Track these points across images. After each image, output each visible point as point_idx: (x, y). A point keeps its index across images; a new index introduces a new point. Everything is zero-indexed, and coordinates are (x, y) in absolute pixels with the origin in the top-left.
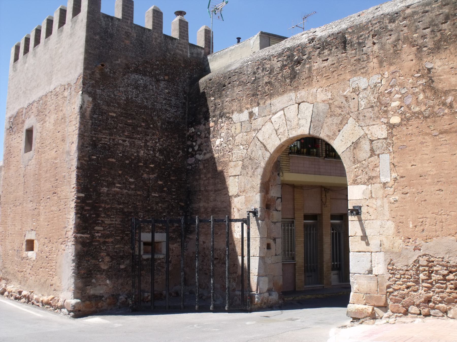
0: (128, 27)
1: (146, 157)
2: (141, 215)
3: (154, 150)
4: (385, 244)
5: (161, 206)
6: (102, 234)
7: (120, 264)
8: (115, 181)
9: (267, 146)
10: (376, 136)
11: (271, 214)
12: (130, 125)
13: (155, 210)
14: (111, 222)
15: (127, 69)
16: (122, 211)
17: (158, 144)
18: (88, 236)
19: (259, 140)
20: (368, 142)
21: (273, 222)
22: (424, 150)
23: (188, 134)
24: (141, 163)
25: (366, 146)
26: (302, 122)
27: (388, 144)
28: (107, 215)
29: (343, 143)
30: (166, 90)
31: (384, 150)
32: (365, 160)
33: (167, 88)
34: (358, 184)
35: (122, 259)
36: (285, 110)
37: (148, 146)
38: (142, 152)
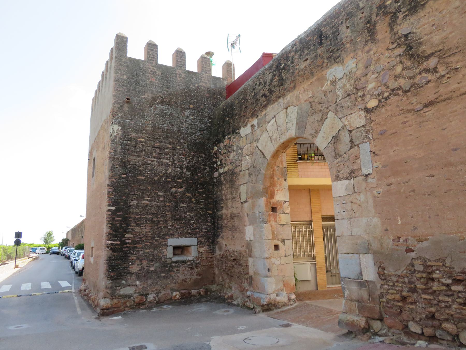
0: (153, 66)
1: (174, 173)
2: (169, 223)
3: (181, 167)
4: (373, 245)
5: (189, 215)
6: (132, 240)
7: (149, 267)
8: (144, 195)
9: (264, 153)
10: (355, 126)
12: (157, 148)
13: (183, 219)
15: (153, 101)
16: (151, 220)
17: (185, 163)
18: (118, 243)
20: (347, 134)
21: (280, 225)
23: (213, 152)
25: (345, 137)
26: (290, 125)
27: (367, 132)
29: (325, 139)
31: (364, 139)
32: (345, 153)
33: (192, 116)
34: (340, 179)
35: (152, 262)
37: (175, 164)
38: (170, 169)
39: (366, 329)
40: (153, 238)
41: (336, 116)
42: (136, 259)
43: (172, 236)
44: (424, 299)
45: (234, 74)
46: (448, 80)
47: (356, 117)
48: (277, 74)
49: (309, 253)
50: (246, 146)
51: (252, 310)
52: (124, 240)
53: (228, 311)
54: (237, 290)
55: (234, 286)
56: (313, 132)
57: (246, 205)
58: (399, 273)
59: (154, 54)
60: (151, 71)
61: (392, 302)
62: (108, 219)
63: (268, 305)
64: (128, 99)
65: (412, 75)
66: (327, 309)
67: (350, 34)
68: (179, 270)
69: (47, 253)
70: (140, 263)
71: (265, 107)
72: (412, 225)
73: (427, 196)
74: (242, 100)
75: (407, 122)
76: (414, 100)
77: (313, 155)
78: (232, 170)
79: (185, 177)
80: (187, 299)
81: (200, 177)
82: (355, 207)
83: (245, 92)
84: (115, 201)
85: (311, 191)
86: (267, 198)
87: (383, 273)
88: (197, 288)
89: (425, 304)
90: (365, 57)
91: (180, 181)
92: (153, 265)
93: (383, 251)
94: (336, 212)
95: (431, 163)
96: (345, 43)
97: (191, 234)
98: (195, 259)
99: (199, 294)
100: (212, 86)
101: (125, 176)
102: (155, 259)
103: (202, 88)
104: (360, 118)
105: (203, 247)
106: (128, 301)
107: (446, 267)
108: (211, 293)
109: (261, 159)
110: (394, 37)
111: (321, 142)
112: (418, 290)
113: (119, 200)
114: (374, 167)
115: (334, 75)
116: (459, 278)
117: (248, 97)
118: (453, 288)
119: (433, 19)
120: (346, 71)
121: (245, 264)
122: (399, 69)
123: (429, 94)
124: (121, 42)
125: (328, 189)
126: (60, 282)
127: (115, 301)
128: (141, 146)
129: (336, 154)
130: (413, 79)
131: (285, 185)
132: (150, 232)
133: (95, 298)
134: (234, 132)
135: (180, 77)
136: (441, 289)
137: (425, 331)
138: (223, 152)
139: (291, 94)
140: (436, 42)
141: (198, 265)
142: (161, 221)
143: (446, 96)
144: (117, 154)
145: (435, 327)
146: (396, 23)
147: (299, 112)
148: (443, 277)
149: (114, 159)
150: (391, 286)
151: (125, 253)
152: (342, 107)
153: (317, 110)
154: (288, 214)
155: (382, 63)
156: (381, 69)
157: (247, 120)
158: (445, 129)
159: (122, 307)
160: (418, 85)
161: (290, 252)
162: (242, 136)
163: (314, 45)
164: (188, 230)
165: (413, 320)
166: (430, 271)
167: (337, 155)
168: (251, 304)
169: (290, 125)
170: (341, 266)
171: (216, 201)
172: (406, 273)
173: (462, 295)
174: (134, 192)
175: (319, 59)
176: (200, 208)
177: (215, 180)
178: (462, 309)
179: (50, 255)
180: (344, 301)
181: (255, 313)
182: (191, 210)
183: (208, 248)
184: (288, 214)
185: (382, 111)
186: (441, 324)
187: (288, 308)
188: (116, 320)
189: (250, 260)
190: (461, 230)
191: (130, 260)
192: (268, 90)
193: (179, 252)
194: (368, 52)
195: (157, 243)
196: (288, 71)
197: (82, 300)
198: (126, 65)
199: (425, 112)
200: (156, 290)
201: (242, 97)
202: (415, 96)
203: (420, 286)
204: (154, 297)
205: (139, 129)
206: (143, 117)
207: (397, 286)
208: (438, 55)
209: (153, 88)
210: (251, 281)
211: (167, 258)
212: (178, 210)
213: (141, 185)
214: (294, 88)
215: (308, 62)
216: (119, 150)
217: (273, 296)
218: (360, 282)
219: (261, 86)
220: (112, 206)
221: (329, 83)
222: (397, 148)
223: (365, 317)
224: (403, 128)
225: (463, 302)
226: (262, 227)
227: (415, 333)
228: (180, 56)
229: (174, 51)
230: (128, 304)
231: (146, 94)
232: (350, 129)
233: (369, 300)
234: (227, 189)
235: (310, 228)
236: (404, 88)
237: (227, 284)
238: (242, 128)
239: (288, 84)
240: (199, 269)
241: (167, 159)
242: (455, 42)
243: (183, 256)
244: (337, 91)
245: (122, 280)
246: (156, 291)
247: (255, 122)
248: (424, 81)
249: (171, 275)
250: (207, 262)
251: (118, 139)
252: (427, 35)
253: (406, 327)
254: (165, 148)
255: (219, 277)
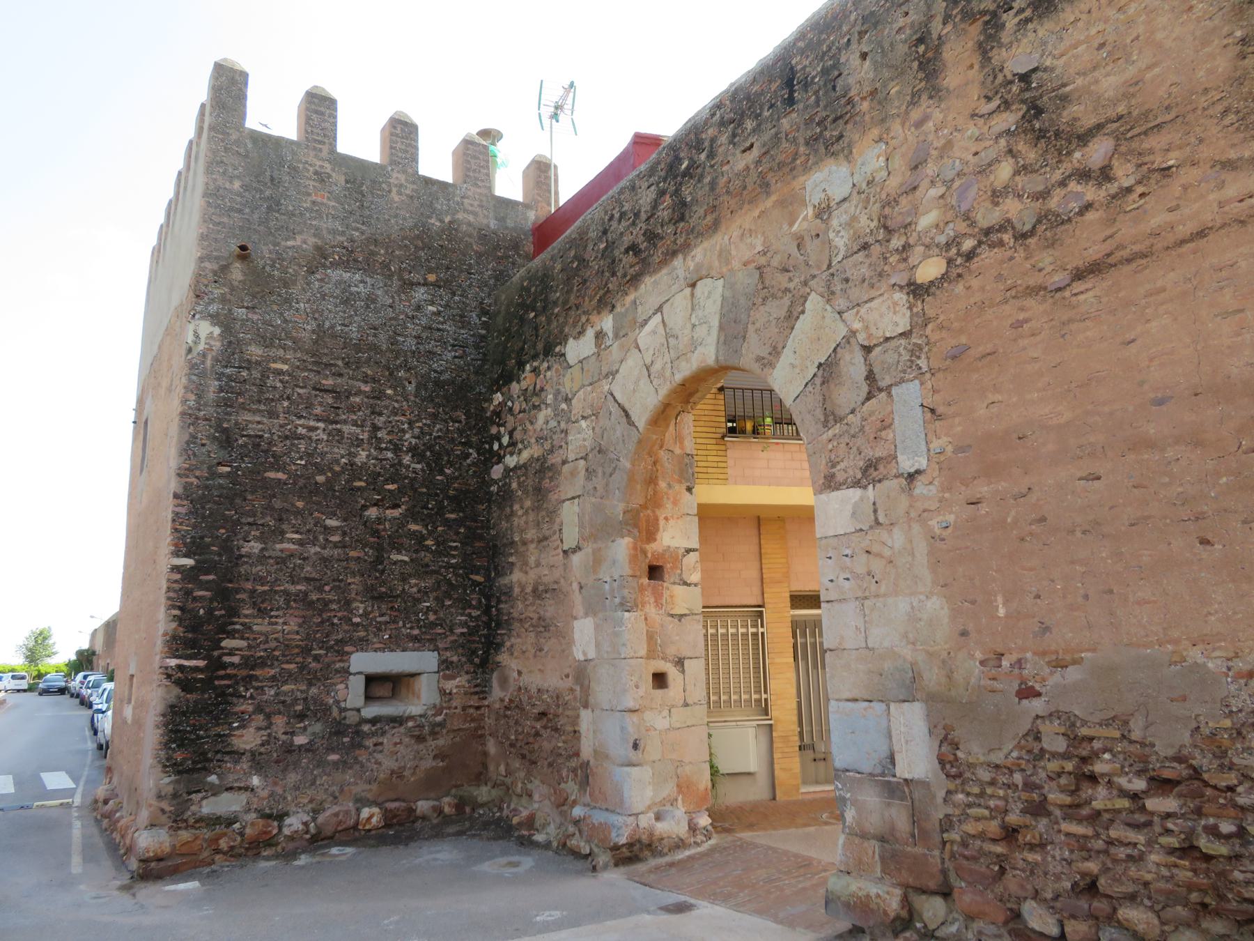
0: (323, 160)
1: (375, 466)
3: (397, 449)
4: (926, 675)
5: (416, 585)
6: (242, 657)
7: (293, 734)
8: (284, 527)
9: (630, 413)
11: (666, 594)
13: (398, 596)
14: (269, 628)
15: (320, 259)
16: (303, 598)
17: (407, 436)
18: (201, 663)
19: (616, 401)
20: (859, 356)
21: (672, 616)
22: (1024, 349)
24: (360, 480)
25: (853, 366)
26: (701, 332)
27: (915, 351)
28: (259, 610)
29: (797, 370)
30: (430, 308)
32: (853, 412)
33: (432, 303)
35: (302, 721)
36: (666, 308)
37: (380, 440)
38: (364, 454)
39: (903, 920)
40: (306, 651)
41: (828, 307)
42: (254, 713)
43: (363, 644)
44: (1068, 834)
45: (557, 193)
46: (1142, 201)
47: (884, 309)
48: (670, 189)
49: (754, 696)
50: (581, 393)
51: (584, 861)
52: (220, 657)
53: (516, 865)
54: (547, 802)
55: (539, 789)
56: (764, 352)
57: (576, 559)
58: (997, 758)
59: (327, 125)
60: (316, 173)
61: (978, 842)
62: (172, 594)
63: (630, 845)
64: (243, 248)
65: (1041, 188)
66: (796, 856)
67: (871, 75)
68: (381, 744)
69: (31, 689)
70: (265, 724)
71: (635, 280)
72: (1036, 619)
73: (1079, 534)
74: (572, 262)
75: (1026, 321)
76: (1046, 259)
77: (768, 420)
78: (542, 460)
79: (406, 477)
80: (400, 829)
81: (451, 479)
82: (877, 565)
83: (581, 241)
84: (193, 543)
85: (765, 523)
86: (634, 538)
87: (951, 758)
88: (432, 795)
89: (1072, 851)
90: (910, 138)
91: (390, 487)
92: (305, 728)
93: (953, 693)
94: (825, 581)
95: (1092, 439)
96: (857, 99)
97: (419, 641)
98: (430, 713)
99: (439, 811)
100: (493, 224)
101: (228, 469)
102: (322, 711)
103: (464, 228)
104: (895, 313)
105: (454, 678)
106: (225, 834)
107: (1131, 742)
108: (473, 810)
109: (621, 429)
110: (993, 82)
111: (788, 380)
112: (1051, 808)
113: (207, 540)
114: (932, 452)
115: (824, 190)
116: (1167, 774)
117: (589, 254)
118: (1152, 804)
119: (1100, 28)
120: (857, 178)
121: (569, 728)
122: (1005, 171)
123: (1087, 242)
124: (229, 87)
125: (804, 516)
126: (43, 775)
127: (185, 835)
128: (279, 385)
129: (826, 416)
130: (1044, 199)
131: (690, 503)
132: (298, 633)
133: (127, 828)
134: (548, 351)
135: (399, 193)
136: (1117, 806)
137: (1068, 929)
138: (517, 408)
139: (706, 244)
140: (1111, 93)
141: (437, 729)
142: (331, 601)
143: (1136, 248)
144: (206, 405)
145: (1097, 918)
146: (999, 42)
147: (728, 294)
148: (1123, 772)
149: (197, 418)
150: (976, 795)
151: (222, 693)
152: (847, 280)
153: (775, 291)
154: (696, 585)
155: (958, 154)
156: (954, 172)
157: (584, 319)
158: (1133, 341)
159: (205, 854)
160: (1058, 215)
161: (698, 693)
162: (571, 362)
163: (772, 106)
164: (411, 628)
165: (1036, 895)
166: (1084, 753)
167: (830, 417)
168: (582, 844)
169: (701, 332)
170: (835, 737)
171: (495, 546)
172: (1018, 758)
173: (1175, 824)
174: (254, 516)
175: (785, 144)
176: (449, 566)
177: (494, 488)
178: (1176, 866)
179: (40, 694)
180: (842, 839)
181: (594, 869)
182: (423, 571)
183: (469, 682)
184: (696, 585)
185: (957, 291)
186: (1115, 910)
187: (687, 853)
188: (181, 892)
189: (586, 716)
190: (1175, 634)
191: (236, 714)
192: (644, 235)
193: (380, 691)
194: (919, 124)
195: (319, 666)
196: (699, 181)
197: (95, 830)
198: (242, 150)
199: (1076, 295)
200: (311, 801)
201: (572, 253)
202: (1048, 247)
203: (1056, 797)
204: (306, 824)
205: (274, 336)
206: (287, 301)
207: (991, 796)
208: (1113, 132)
209: (319, 221)
210: (585, 775)
211: (345, 710)
212: (382, 572)
213: (274, 496)
214: (715, 226)
215: (755, 152)
216: (211, 395)
217: (646, 821)
218: (889, 782)
219: (624, 224)
220: (186, 556)
221: (810, 211)
222: (998, 397)
223: (900, 885)
224: (1015, 340)
225: (1177, 846)
226: (620, 622)
227: (1042, 934)
228: (401, 134)
229: (383, 120)
230: (223, 844)
231: (299, 238)
232: (866, 343)
233: (913, 836)
234: (526, 513)
235: (756, 626)
236: (1018, 226)
237: (520, 785)
238: (571, 341)
239: (697, 215)
240: (441, 742)
241: (355, 424)
242: (1162, 92)
243: (395, 702)
244: (832, 235)
245: (210, 773)
246: (310, 806)
247: (607, 323)
248: (1075, 206)
249: (356, 758)
250: (465, 721)
251: (209, 363)
252: (1085, 74)
253: (1017, 915)
254: (350, 394)
255: (498, 766)
